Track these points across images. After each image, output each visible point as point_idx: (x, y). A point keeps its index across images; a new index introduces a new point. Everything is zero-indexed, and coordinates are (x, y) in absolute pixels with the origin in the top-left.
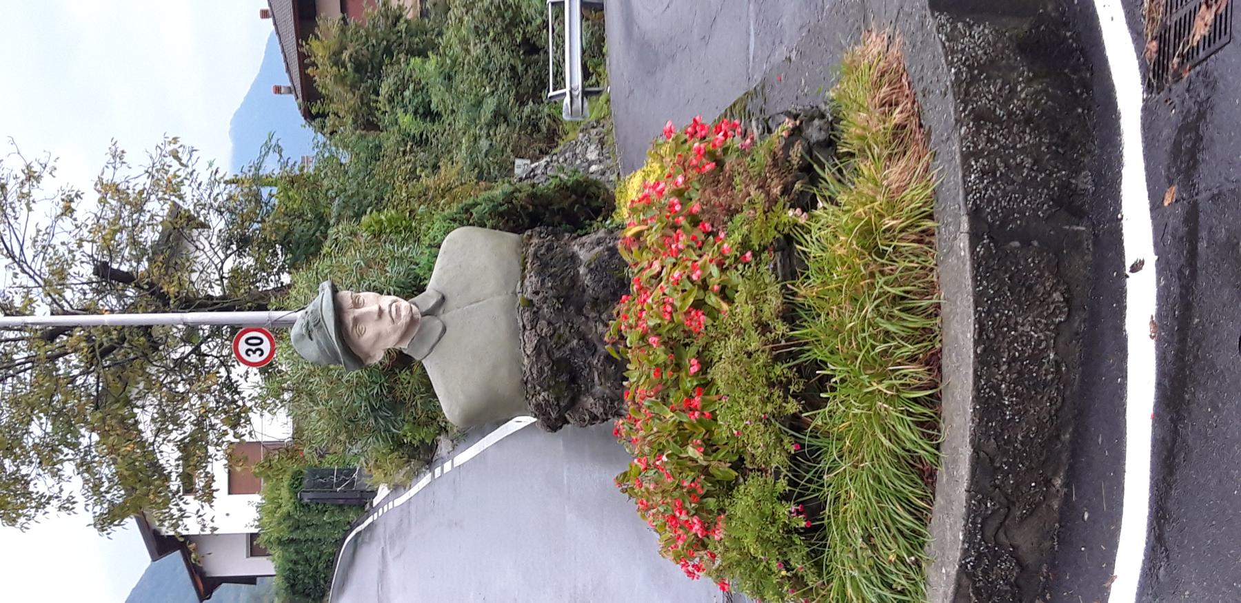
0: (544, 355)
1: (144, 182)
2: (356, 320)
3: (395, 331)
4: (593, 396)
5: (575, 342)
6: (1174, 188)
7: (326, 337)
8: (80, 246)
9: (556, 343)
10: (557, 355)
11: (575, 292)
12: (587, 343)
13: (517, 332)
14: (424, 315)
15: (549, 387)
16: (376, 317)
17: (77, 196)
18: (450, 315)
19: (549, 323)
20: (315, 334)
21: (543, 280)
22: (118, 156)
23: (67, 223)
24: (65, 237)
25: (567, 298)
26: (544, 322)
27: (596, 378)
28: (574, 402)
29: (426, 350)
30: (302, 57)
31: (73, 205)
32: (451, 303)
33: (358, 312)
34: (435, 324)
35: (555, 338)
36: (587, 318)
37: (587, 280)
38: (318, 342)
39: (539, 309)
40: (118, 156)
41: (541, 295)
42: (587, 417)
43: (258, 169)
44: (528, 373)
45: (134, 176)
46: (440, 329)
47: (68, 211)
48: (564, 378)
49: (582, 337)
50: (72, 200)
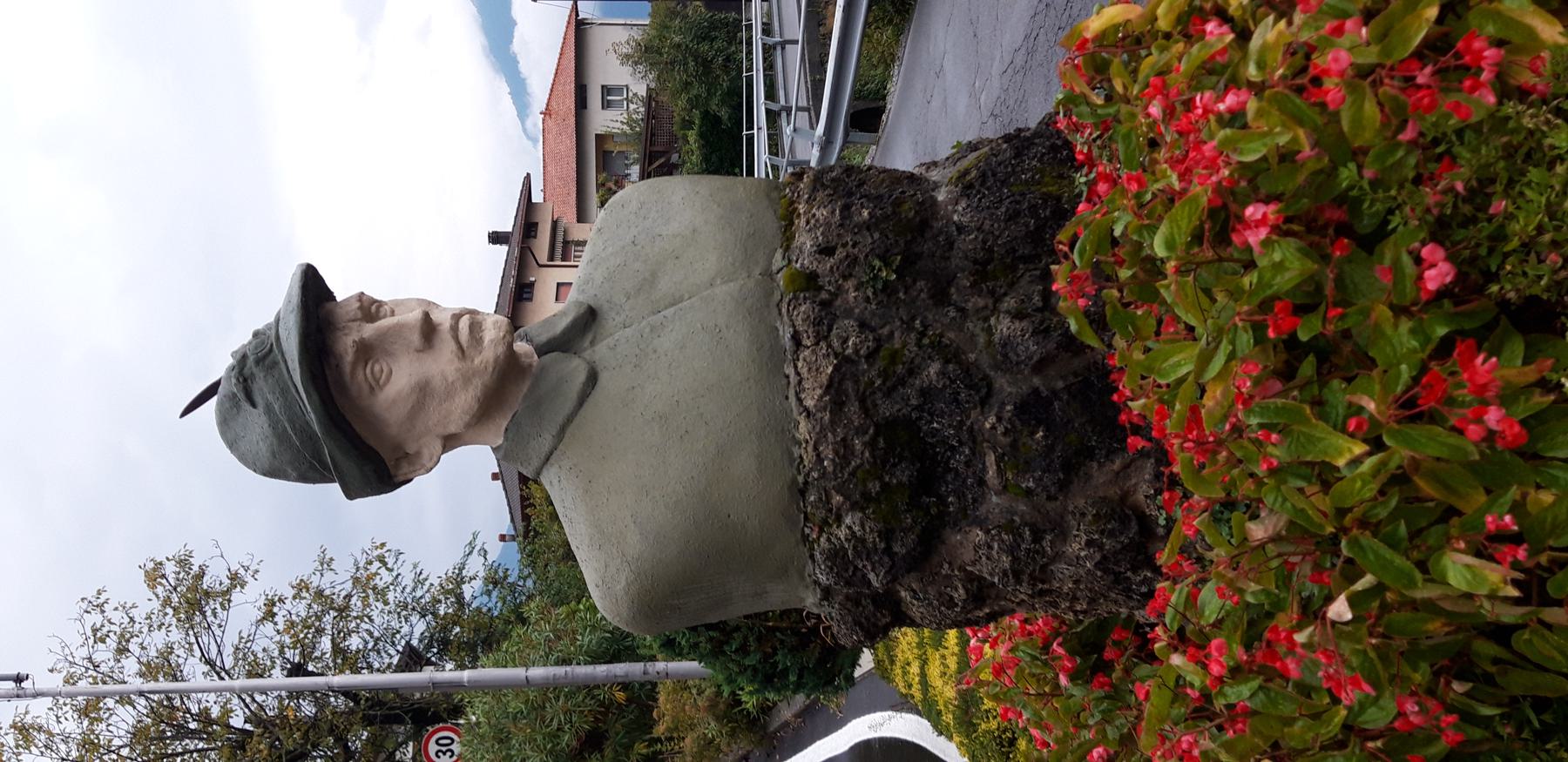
0: (853, 408)
2: (366, 351)
3: (467, 379)
4: (981, 523)
5: (934, 368)
7: (284, 390)
8: (282, 652)
9: (884, 374)
10: (886, 409)
11: (927, 247)
12: (967, 370)
13: (772, 360)
14: (542, 350)
15: (866, 496)
16: (416, 338)
17: (280, 600)
18: (604, 350)
19: (863, 325)
20: (262, 387)
21: (846, 208)
23: (268, 628)
25: (910, 260)
26: (850, 323)
27: (991, 472)
28: (925, 553)
29: (546, 441)
30: (523, 499)
31: (275, 610)
33: (369, 330)
34: (574, 369)
36: (962, 310)
38: (269, 410)
39: (835, 296)
40: (326, 563)
41: (840, 253)
42: (960, 594)
43: (461, 570)
44: (809, 458)
45: (338, 582)
46: (581, 377)
47: (270, 615)
48: (902, 475)
49: (950, 355)
50: (274, 604)
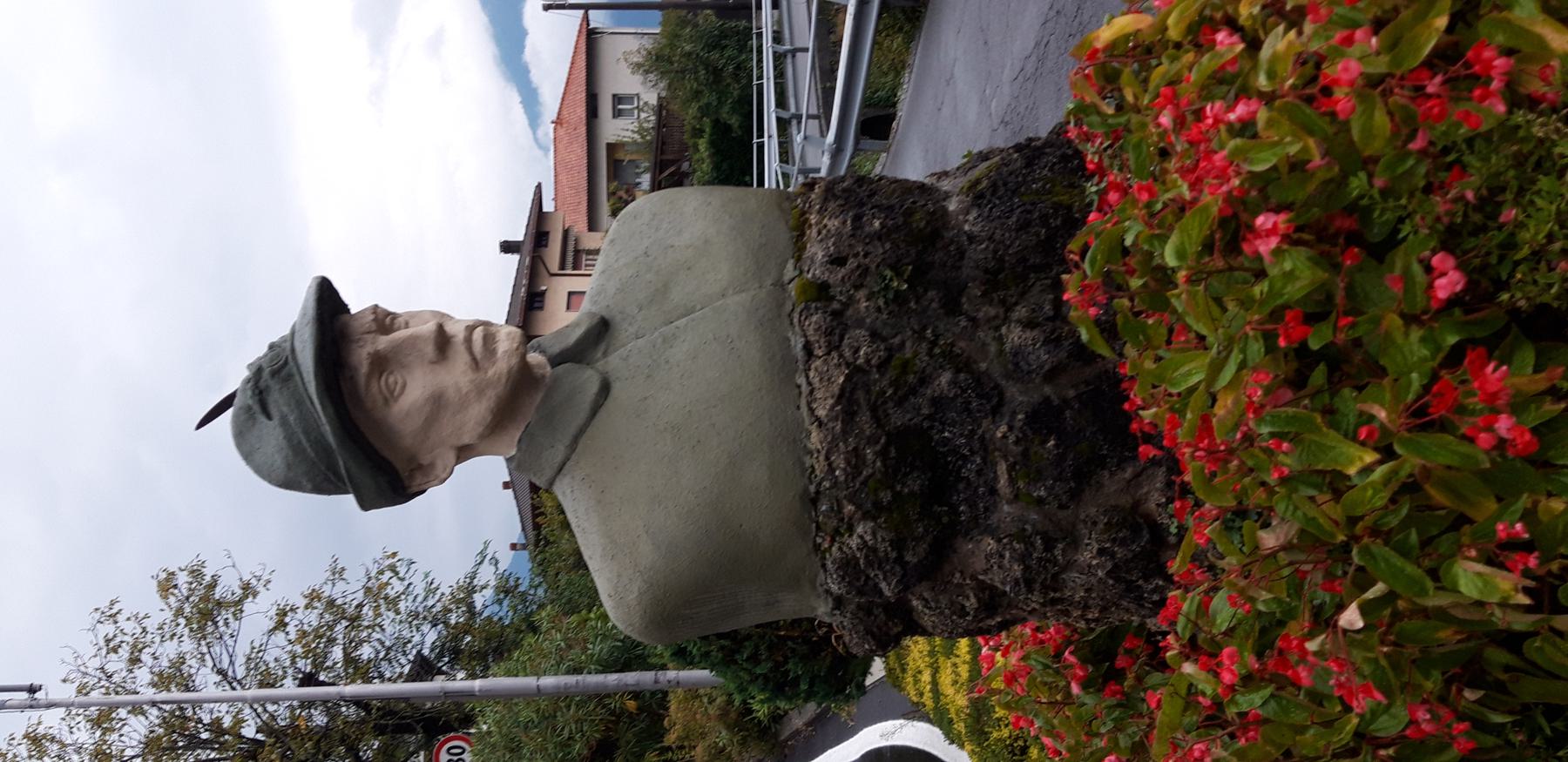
0: (864, 418)
1: (360, 595)
2: (381, 363)
3: (480, 390)
5: (945, 378)
6: (1488, 465)
7: (300, 402)
8: (293, 662)
9: (895, 383)
10: (898, 418)
11: (938, 256)
13: (784, 369)
14: (556, 361)
15: (877, 505)
16: (430, 350)
19: (874, 335)
20: (277, 400)
21: (857, 218)
22: (338, 573)
23: (280, 638)
24: (276, 653)
26: (861, 333)
27: (1003, 481)
28: (935, 565)
30: (534, 508)
31: (287, 620)
32: (624, 330)
33: (383, 342)
35: (891, 373)
36: (973, 320)
37: (971, 223)
38: (284, 422)
40: (338, 573)
41: (852, 263)
42: (971, 603)
43: (473, 578)
44: (820, 467)
45: (350, 591)
48: (914, 484)
